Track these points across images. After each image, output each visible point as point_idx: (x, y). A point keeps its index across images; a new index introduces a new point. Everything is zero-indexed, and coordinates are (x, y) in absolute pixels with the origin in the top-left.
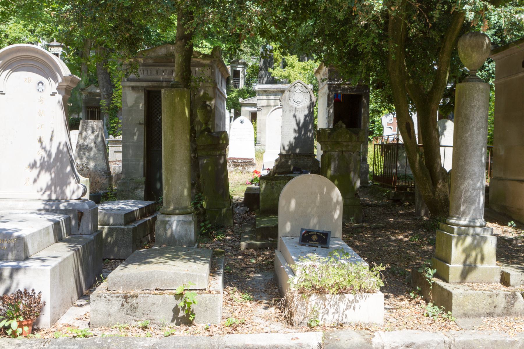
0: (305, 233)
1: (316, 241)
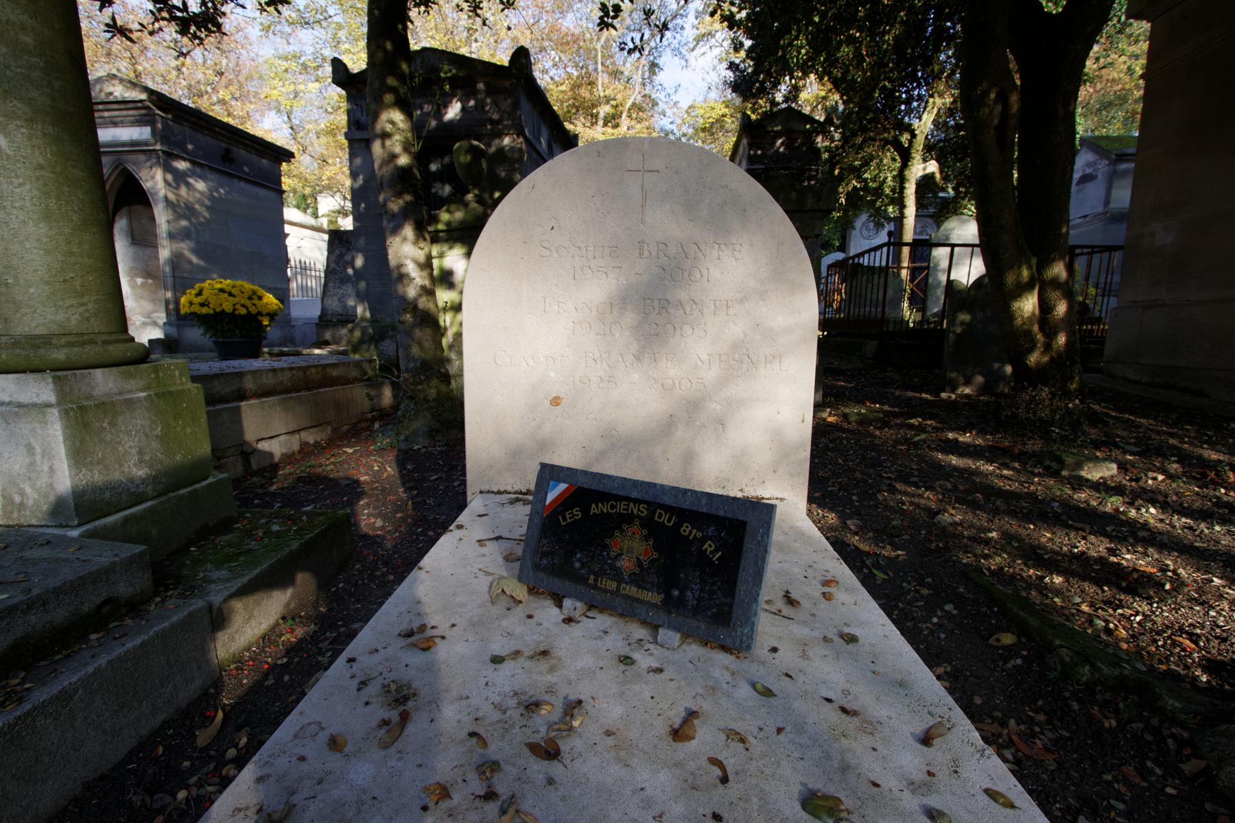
0: (565, 502)
1: (638, 580)
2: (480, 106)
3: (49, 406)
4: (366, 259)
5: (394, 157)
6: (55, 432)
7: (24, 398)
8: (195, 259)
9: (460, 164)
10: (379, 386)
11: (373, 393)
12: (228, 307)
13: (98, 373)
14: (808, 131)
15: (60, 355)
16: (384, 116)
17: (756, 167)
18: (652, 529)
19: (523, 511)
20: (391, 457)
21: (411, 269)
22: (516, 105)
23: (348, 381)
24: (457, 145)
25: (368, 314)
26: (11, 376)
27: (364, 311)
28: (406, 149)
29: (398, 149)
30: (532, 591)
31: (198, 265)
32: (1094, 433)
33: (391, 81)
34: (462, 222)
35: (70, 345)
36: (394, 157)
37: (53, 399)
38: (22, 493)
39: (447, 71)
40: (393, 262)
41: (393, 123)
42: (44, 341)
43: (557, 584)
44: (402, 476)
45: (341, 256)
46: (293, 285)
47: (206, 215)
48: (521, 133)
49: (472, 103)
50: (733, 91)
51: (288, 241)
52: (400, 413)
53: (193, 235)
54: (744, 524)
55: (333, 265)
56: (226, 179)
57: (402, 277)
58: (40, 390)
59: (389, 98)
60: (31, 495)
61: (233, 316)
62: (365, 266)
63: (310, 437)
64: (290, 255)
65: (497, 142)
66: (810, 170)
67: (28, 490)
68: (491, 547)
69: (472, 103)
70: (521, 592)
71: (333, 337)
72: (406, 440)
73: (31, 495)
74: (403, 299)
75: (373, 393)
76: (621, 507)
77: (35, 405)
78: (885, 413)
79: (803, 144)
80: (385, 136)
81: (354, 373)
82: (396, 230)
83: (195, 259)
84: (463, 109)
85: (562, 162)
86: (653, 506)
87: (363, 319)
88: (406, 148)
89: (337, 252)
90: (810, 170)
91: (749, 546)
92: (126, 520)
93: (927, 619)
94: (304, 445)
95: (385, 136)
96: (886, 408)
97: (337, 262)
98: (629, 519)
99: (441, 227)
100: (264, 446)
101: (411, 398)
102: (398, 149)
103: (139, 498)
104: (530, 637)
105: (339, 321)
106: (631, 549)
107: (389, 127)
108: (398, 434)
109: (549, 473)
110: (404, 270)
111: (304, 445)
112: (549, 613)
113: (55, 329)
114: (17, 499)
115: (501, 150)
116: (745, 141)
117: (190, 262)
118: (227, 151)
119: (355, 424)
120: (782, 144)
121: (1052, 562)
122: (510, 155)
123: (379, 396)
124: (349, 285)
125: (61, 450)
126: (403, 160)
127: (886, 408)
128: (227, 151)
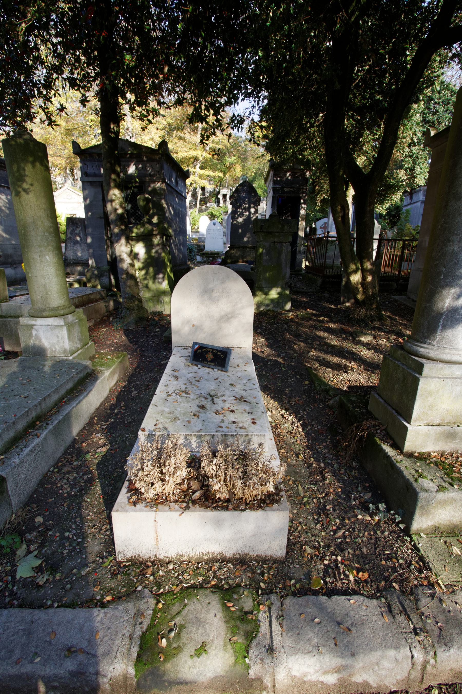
2: (144, 168)
3: (63, 326)
4: (92, 238)
5: (116, 210)
6: (65, 332)
7: (55, 324)
8: (4, 235)
9: (141, 206)
10: (108, 302)
11: (107, 304)
13: (69, 316)
14: (302, 169)
15: (62, 312)
16: (111, 192)
17: (277, 186)
19: (190, 350)
20: (122, 332)
21: (125, 256)
22: (162, 168)
23: (97, 301)
24: (138, 197)
25: (94, 265)
26: (52, 318)
27: (93, 263)
28: (121, 206)
29: (118, 207)
30: (192, 364)
31: (6, 238)
32: (377, 324)
33: (113, 176)
34: (143, 232)
35: (63, 309)
36: (116, 210)
37: (63, 324)
38: (55, 348)
41: (115, 195)
43: (196, 363)
44: (129, 340)
47: (8, 212)
48: (164, 181)
49: (140, 166)
50: (266, 149)
52: (122, 314)
53: (3, 222)
54: (227, 352)
57: (122, 260)
58: (59, 321)
59: (112, 184)
60: (58, 348)
62: (92, 242)
65: (152, 185)
66: (303, 189)
67: (57, 347)
68: (182, 358)
69: (140, 166)
70: (190, 364)
71: (71, 271)
72: (126, 325)
73: (58, 348)
74: (122, 269)
75: (107, 304)
76: (205, 350)
77: (59, 326)
78: (312, 314)
79: (300, 175)
80: (112, 201)
81: (98, 296)
82: (118, 241)
83: (4, 235)
84: (137, 168)
86: (213, 349)
87: (92, 267)
89: (71, 229)
90: (303, 189)
91: (228, 356)
92: (79, 355)
93: (291, 379)
95: (112, 201)
96: (314, 312)
97: (71, 233)
98: (209, 351)
101: (128, 309)
102: (118, 207)
104: (193, 371)
105: (73, 263)
107: (114, 197)
108: (123, 323)
109: (195, 344)
110: (122, 257)
112: (195, 368)
113: (59, 305)
114: (54, 349)
116: (272, 173)
117: (3, 236)
119: (102, 318)
120: (290, 175)
121: (327, 364)
122: (159, 191)
123: (109, 305)
124: (78, 245)
125: (66, 337)
126: (120, 211)
127: (314, 312)
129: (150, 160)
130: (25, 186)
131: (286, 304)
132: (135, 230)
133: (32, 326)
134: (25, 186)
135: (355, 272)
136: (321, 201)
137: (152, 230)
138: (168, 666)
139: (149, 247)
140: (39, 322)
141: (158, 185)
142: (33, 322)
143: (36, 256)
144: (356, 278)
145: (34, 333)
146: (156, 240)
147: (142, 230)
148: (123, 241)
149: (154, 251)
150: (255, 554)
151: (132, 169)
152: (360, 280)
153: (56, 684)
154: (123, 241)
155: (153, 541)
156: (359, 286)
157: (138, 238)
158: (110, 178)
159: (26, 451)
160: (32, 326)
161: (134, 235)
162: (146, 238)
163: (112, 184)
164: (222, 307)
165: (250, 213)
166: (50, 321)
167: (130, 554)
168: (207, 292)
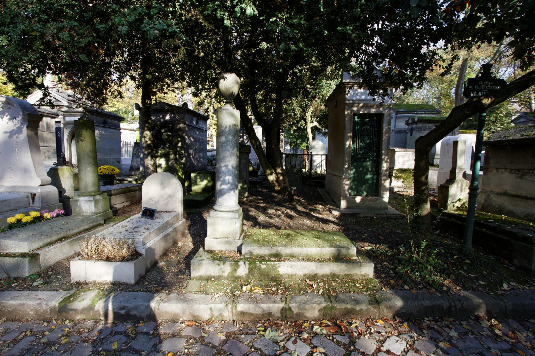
2: (175, 117)
6: (93, 203)
12: (107, 173)
15: (93, 194)
16: (145, 133)
18: (150, 212)
29: (148, 140)
36: (147, 142)
39: (167, 108)
40: (146, 165)
42: (91, 192)
45: (137, 150)
46: (123, 150)
49: (172, 115)
51: (121, 135)
55: (135, 152)
56: (104, 129)
58: (92, 198)
59: (146, 128)
61: (108, 175)
63: (125, 204)
64: (122, 140)
69: (172, 115)
84: (170, 117)
85: (155, 174)
88: (150, 139)
94: (124, 206)
95: (145, 137)
97: (136, 151)
99: (159, 154)
100: (115, 206)
102: (148, 140)
103: (101, 213)
106: (148, 213)
107: (146, 135)
111: (124, 206)
115: (180, 128)
118: (105, 120)
126: (149, 142)
128: (105, 120)
129: (177, 113)
130: (81, 138)
131: (245, 193)
132: (160, 152)
133: (78, 201)
134: (81, 138)
135: (271, 174)
136: (312, 128)
137: (169, 152)
138: (70, 304)
139: (167, 161)
140: (82, 198)
141: (181, 125)
142: (79, 199)
143: (83, 168)
144: (272, 178)
145: (78, 204)
146: (172, 157)
147: (163, 151)
148: (149, 158)
149: (170, 163)
150: (123, 281)
151: (168, 117)
152: (275, 179)
153: (32, 308)
154: (149, 158)
155: (84, 274)
156: (275, 182)
157: (162, 156)
158: (145, 126)
159: (52, 247)
160: (78, 201)
161: (159, 154)
162: (166, 156)
163: (146, 128)
164: (168, 191)
165: (243, 139)
166: (87, 198)
167: (76, 280)
168: (163, 185)
